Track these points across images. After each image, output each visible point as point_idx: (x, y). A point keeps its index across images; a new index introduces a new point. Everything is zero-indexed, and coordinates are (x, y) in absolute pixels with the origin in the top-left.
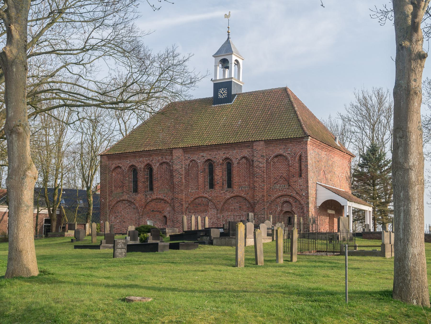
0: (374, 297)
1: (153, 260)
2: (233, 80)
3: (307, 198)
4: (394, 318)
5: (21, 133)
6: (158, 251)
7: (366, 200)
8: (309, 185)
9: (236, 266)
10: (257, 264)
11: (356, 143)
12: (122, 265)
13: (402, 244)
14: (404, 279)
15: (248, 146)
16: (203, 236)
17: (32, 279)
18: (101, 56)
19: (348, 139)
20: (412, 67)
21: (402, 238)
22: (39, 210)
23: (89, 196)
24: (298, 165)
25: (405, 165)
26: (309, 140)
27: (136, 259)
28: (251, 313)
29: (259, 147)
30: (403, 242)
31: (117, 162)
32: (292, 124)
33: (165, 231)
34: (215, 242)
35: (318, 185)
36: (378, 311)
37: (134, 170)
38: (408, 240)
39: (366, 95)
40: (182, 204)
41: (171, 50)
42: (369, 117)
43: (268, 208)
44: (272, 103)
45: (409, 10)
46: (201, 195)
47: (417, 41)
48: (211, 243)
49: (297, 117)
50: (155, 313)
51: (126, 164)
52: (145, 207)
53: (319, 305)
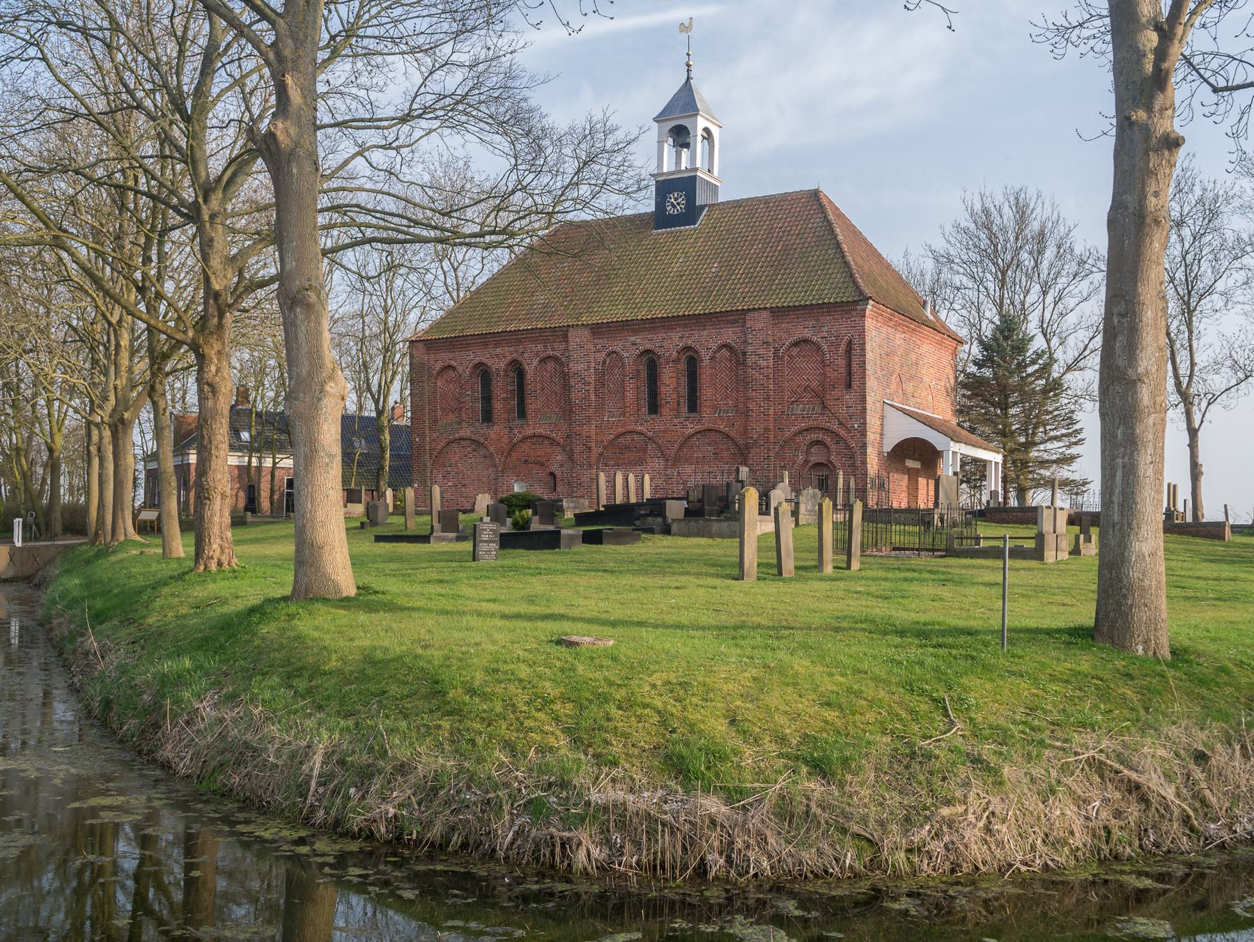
0: (1057, 638)
1: (559, 566)
2: (698, 174)
3: (863, 433)
4: (1101, 680)
5: (313, 305)
6: (559, 548)
7: (987, 438)
8: (868, 407)
9: (740, 577)
10: (780, 573)
11: (964, 312)
12: (504, 576)
13: (1117, 533)
14: (1119, 604)
15: (735, 321)
16: (646, 515)
17: (346, 603)
18: (435, 130)
19: (947, 303)
20: (1151, 165)
21: (1116, 521)
22: (277, 460)
23: (380, 430)
24: (844, 362)
25: (1130, 372)
26: (869, 307)
27: (525, 564)
28: (819, 668)
29: (760, 322)
30: (1120, 530)
31: (445, 358)
32: (830, 271)
33: (562, 506)
34: (674, 528)
35: (886, 406)
36: (1069, 666)
37: (484, 373)
38: (1129, 525)
39: (989, 204)
40: (590, 448)
41: (598, 116)
42: (992, 254)
43: (777, 456)
44: (786, 225)
45: (1146, 42)
47: (1163, 109)
48: (667, 531)
49: (843, 257)
50: (632, 668)
51: (465, 361)
52: (509, 454)
53: (950, 654)
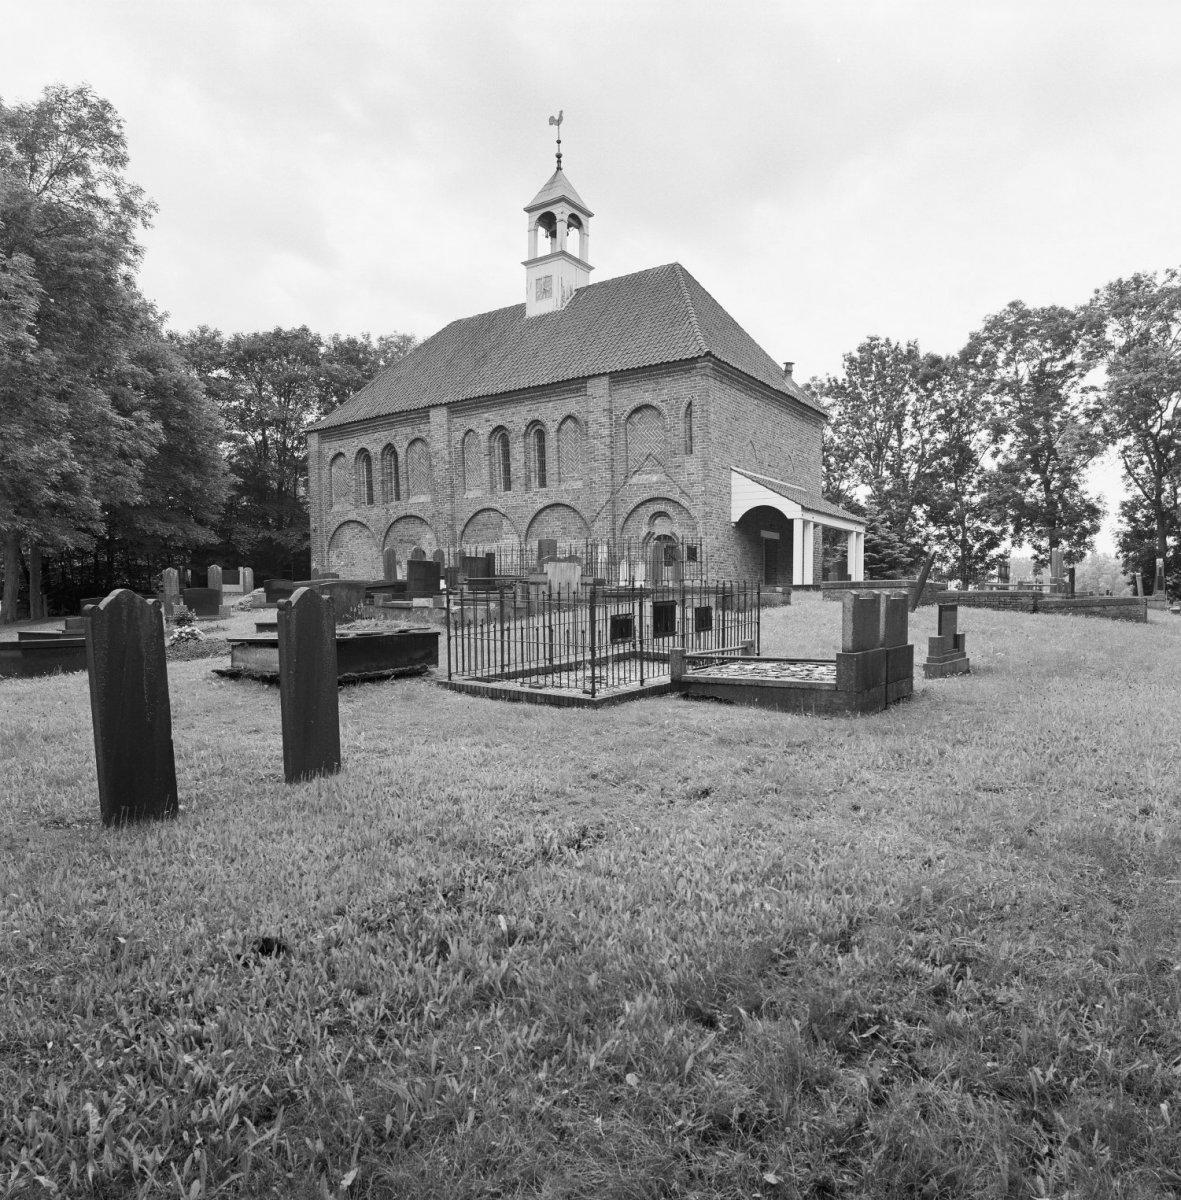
46: (486, 506)
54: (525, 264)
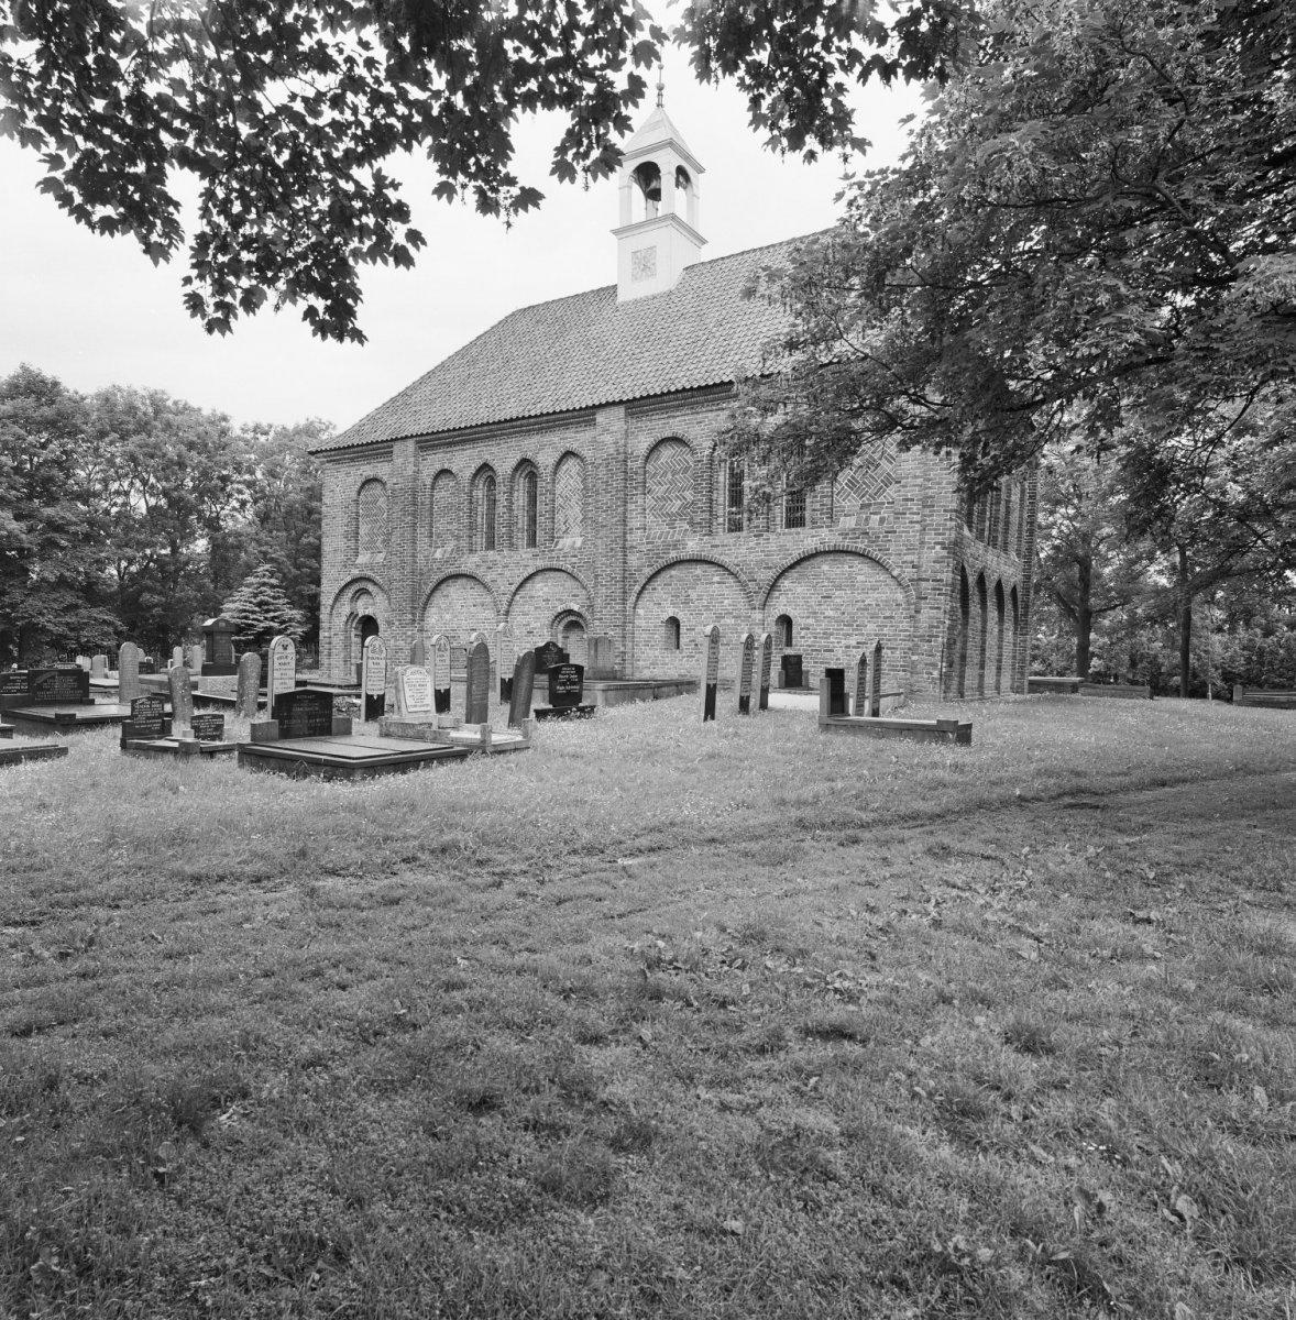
54: (616, 232)
